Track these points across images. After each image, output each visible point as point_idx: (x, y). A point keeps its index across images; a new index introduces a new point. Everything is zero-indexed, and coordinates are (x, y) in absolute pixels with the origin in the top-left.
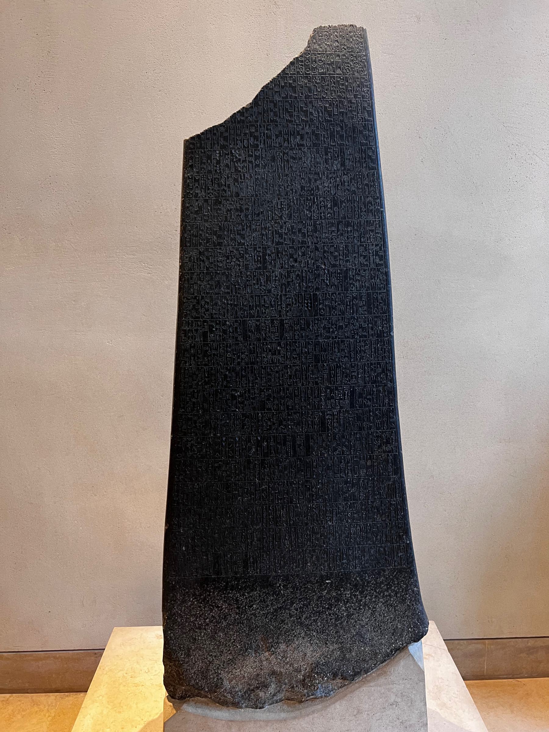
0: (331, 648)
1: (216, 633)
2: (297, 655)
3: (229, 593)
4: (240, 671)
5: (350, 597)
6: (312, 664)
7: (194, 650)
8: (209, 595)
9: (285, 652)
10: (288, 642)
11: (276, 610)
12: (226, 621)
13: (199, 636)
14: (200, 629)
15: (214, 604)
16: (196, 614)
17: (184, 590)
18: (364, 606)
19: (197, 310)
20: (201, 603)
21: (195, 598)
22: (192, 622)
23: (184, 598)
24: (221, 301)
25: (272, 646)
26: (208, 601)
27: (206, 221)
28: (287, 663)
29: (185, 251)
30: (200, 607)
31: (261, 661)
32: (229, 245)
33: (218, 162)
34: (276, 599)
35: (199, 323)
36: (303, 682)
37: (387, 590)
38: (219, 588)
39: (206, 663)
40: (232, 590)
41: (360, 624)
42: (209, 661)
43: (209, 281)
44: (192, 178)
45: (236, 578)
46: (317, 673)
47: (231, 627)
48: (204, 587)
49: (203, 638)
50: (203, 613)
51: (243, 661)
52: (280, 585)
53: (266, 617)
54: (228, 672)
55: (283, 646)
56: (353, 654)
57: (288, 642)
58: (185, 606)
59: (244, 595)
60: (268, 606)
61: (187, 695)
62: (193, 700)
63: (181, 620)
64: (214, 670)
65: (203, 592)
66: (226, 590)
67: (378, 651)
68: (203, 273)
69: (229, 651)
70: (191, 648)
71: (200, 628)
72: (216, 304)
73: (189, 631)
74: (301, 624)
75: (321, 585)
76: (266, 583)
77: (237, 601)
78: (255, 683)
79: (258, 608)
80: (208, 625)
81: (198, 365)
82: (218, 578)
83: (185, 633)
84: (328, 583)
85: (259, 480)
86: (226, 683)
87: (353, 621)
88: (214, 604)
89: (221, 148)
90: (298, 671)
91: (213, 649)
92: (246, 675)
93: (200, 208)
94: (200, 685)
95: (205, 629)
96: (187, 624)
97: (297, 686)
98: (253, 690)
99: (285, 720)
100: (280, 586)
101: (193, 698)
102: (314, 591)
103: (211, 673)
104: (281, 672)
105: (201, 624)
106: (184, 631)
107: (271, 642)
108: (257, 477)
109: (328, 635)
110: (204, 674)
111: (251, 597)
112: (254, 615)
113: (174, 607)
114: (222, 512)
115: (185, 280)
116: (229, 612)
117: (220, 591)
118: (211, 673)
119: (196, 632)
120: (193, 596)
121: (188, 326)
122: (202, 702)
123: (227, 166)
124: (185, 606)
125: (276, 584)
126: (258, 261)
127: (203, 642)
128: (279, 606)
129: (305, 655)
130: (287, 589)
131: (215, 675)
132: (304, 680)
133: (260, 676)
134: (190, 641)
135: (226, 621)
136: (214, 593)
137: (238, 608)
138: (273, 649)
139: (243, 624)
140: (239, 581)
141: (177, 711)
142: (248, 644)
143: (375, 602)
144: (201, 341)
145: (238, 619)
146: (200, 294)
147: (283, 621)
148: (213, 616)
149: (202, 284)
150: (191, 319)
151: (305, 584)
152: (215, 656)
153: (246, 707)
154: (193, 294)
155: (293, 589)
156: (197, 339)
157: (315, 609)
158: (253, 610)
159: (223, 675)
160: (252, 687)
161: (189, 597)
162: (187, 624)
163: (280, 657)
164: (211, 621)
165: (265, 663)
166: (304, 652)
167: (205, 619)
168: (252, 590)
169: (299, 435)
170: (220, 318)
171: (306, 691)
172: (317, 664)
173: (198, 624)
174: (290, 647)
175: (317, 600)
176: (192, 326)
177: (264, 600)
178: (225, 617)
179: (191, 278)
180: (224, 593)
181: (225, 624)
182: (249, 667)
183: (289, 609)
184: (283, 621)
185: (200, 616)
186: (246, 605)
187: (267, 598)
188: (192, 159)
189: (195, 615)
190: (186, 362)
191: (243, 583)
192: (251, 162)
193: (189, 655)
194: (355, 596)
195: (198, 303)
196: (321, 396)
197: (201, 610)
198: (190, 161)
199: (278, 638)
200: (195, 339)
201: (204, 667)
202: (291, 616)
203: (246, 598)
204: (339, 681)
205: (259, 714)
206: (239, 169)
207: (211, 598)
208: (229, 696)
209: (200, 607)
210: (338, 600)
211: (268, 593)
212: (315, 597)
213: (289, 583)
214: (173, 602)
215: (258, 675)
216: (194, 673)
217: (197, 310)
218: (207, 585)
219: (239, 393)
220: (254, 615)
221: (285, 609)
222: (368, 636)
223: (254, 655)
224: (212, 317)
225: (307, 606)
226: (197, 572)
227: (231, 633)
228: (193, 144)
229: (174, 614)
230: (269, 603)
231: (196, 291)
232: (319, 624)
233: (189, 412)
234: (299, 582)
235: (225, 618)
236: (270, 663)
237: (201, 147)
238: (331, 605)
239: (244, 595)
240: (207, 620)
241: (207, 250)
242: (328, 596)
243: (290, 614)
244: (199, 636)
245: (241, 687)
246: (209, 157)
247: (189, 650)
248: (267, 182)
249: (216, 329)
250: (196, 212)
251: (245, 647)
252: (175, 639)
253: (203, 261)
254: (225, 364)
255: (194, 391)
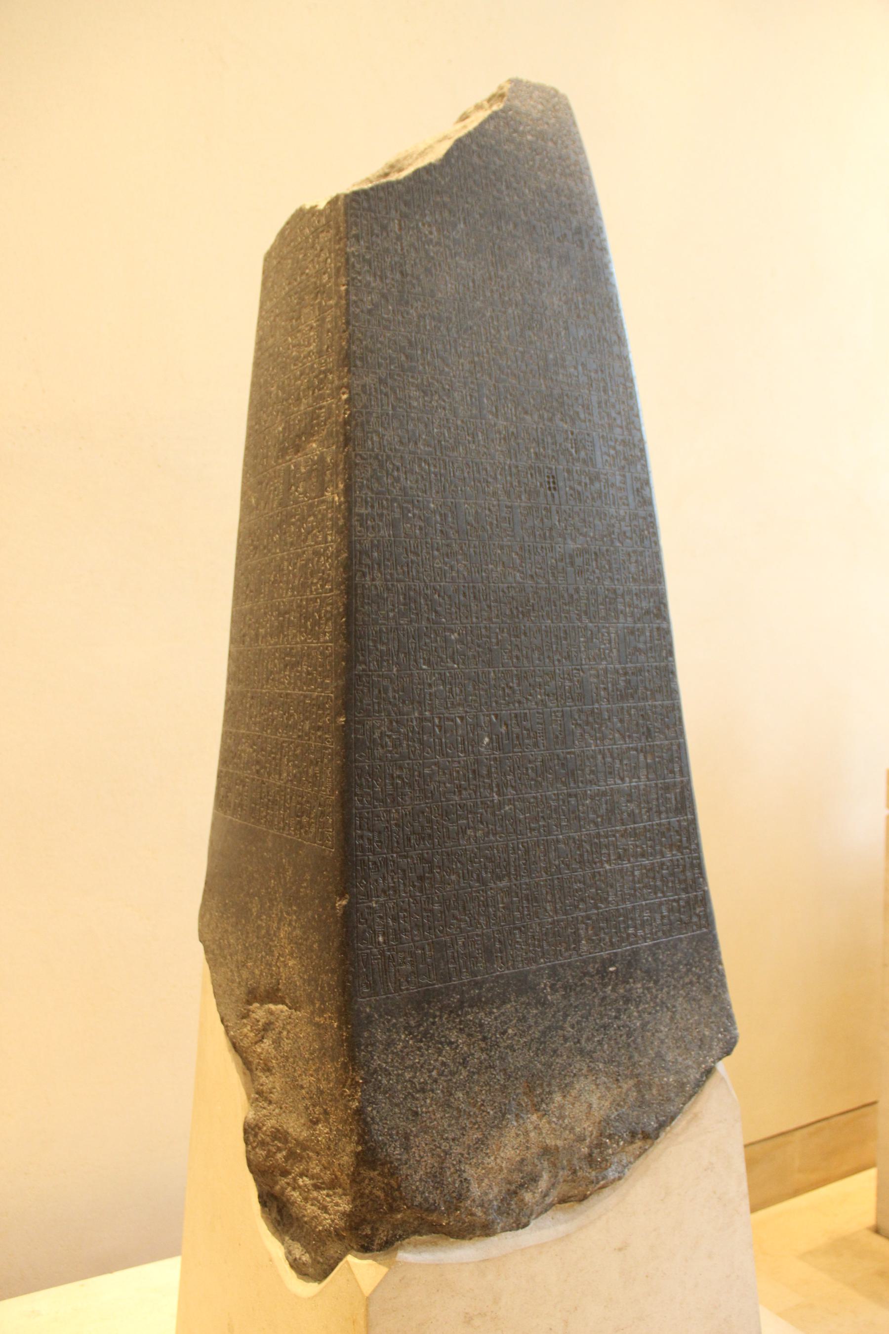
0: (625, 1086)
1: (451, 1094)
2: (579, 1110)
3: (467, 1013)
4: (496, 1158)
5: (643, 993)
6: (599, 1123)
7: (416, 1136)
8: (434, 1023)
9: (561, 1107)
10: (565, 1089)
11: (543, 1033)
12: (465, 1067)
13: (422, 1106)
14: (424, 1092)
15: (443, 1039)
16: (414, 1063)
17: (389, 1021)
18: (661, 1007)
19: (378, 480)
20: (421, 1041)
21: (410, 1033)
22: (406, 1081)
23: (390, 1036)
24: (420, 466)
25: (542, 1100)
26: (433, 1035)
27: (387, 328)
28: (565, 1129)
29: (354, 374)
30: (419, 1049)
31: (527, 1133)
32: (426, 373)
33: (399, 238)
34: (541, 1013)
35: (385, 502)
36: (590, 1159)
37: (686, 974)
38: (449, 1006)
39: (440, 1156)
40: (471, 1006)
41: (659, 1038)
42: (444, 1151)
43: (397, 428)
44: (359, 256)
45: (476, 983)
46: (610, 1137)
47: (476, 1077)
48: (423, 1009)
49: (431, 1109)
50: (425, 1061)
51: (499, 1137)
52: (545, 985)
53: (530, 1049)
54: (477, 1166)
55: (558, 1098)
56: (654, 1091)
57: (565, 1089)
58: (393, 1053)
59: (491, 1013)
60: (530, 1027)
61: (395, 1235)
62: (409, 1243)
63: (388, 1081)
64: (454, 1165)
65: (422, 1018)
66: (462, 1008)
67: (685, 1080)
68: (388, 414)
69: (475, 1124)
70: (412, 1131)
71: (423, 1090)
72: (412, 471)
73: (405, 1099)
74: (581, 1051)
75: (603, 978)
76: (523, 985)
77: (481, 1025)
78: (517, 1177)
79: (515, 1034)
80: (436, 1081)
81: (386, 580)
82: (447, 988)
83: (397, 1105)
84: (612, 972)
85: (499, 795)
86: (476, 1191)
87: (649, 1034)
88: (443, 1039)
89: (401, 216)
90: (581, 1139)
91: (449, 1125)
92: (504, 1165)
93: (376, 306)
94: (431, 1201)
95: (432, 1091)
96: (399, 1087)
97: (580, 1168)
98: (515, 1193)
99: (568, 1236)
100: (545, 988)
101: (407, 1240)
102: (595, 990)
103: (448, 1173)
104: (557, 1148)
105: (425, 1083)
106: (396, 1101)
107: (540, 1094)
108: (495, 789)
109: (619, 1065)
110: (437, 1178)
111: (503, 1014)
112: (511, 1048)
113: (372, 1058)
114: (443, 859)
115: (357, 425)
116: (469, 1049)
117: (451, 1012)
118: (448, 1173)
119: (417, 1099)
120: (405, 1028)
121: (366, 509)
122: (424, 1243)
123: (412, 245)
124: (393, 1053)
125: (539, 984)
126: (472, 403)
127: (430, 1118)
128: (547, 1023)
129: (590, 1106)
130: (557, 991)
131: (456, 1176)
132: (590, 1155)
133: (525, 1163)
134: (408, 1118)
135: (465, 1067)
136: (441, 1017)
137: (484, 1039)
138: (544, 1106)
139: (494, 1067)
140: (481, 988)
141: (390, 1268)
142: (505, 1104)
143: (674, 996)
144: (389, 536)
145: (485, 1059)
146: (384, 451)
147: (555, 1051)
148: (444, 1064)
149: (386, 433)
150: (370, 494)
151: (580, 980)
152: (453, 1140)
153: (504, 1230)
154: (373, 450)
155: (565, 989)
156: (382, 532)
157: (598, 1021)
158: (508, 1038)
159: (470, 1172)
160: (513, 1187)
161: (398, 1033)
162: (399, 1087)
163: (554, 1119)
164: (441, 1074)
165: (532, 1134)
166: (588, 1102)
167: (430, 1071)
168: (504, 1003)
169: (555, 712)
170: (418, 496)
171: (594, 1173)
172: (607, 1121)
173: (420, 1083)
174: (569, 1098)
175: (600, 1005)
176: (373, 507)
177: (524, 1017)
178: (464, 1059)
179: (368, 422)
180: (458, 1015)
181: (465, 1073)
182: (507, 1150)
183: (562, 1028)
184: (555, 1051)
185: (422, 1067)
186: (496, 1031)
187: (529, 1013)
188: (356, 225)
189: (412, 1067)
190: (364, 575)
191: (488, 990)
192: (448, 247)
193: (407, 1148)
194: (648, 989)
195: (381, 466)
196: (579, 642)
197: (422, 1056)
198: (354, 228)
199: (549, 1085)
200: (379, 531)
201: (436, 1164)
202: (566, 1039)
203: (496, 1019)
204: (639, 1143)
205: (525, 1237)
206: (432, 254)
207: (437, 1028)
208: (479, 1212)
209: (419, 1049)
210: (627, 1001)
211: (529, 1004)
212: (596, 1000)
213: (558, 980)
214: (370, 1049)
215: (523, 1160)
216: (421, 1180)
217: (378, 480)
218: (429, 1003)
219: (456, 634)
220: (511, 1048)
221: (556, 1028)
222: (669, 1057)
223: (515, 1123)
224: (406, 494)
225: (587, 1019)
226: (408, 982)
227: (477, 1089)
228: (358, 202)
229: (375, 1071)
230: (531, 1021)
231: (376, 445)
232: (606, 1047)
233: (375, 671)
234: (573, 976)
235: (464, 1063)
236: (540, 1134)
237: (370, 209)
238: (618, 1011)
239: (491, 1013)
240: (434, 1073)
241: (391, 376)
242: (614, 996)
243: (564, 1036)
244: (422, 1106)
245: (496, 1190)
246: (384, 228)
247: (407, 1137)
248: (474, 281)
249: (414, 515)
250: (370, 312)
251: (501, 1111)
252: (381, 1120)
253: (386, 394)
254: (430, 581)
255: (381, 630)
